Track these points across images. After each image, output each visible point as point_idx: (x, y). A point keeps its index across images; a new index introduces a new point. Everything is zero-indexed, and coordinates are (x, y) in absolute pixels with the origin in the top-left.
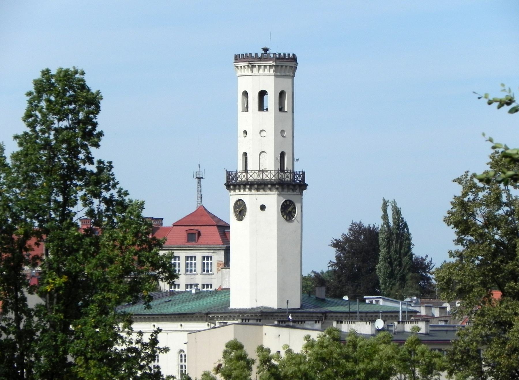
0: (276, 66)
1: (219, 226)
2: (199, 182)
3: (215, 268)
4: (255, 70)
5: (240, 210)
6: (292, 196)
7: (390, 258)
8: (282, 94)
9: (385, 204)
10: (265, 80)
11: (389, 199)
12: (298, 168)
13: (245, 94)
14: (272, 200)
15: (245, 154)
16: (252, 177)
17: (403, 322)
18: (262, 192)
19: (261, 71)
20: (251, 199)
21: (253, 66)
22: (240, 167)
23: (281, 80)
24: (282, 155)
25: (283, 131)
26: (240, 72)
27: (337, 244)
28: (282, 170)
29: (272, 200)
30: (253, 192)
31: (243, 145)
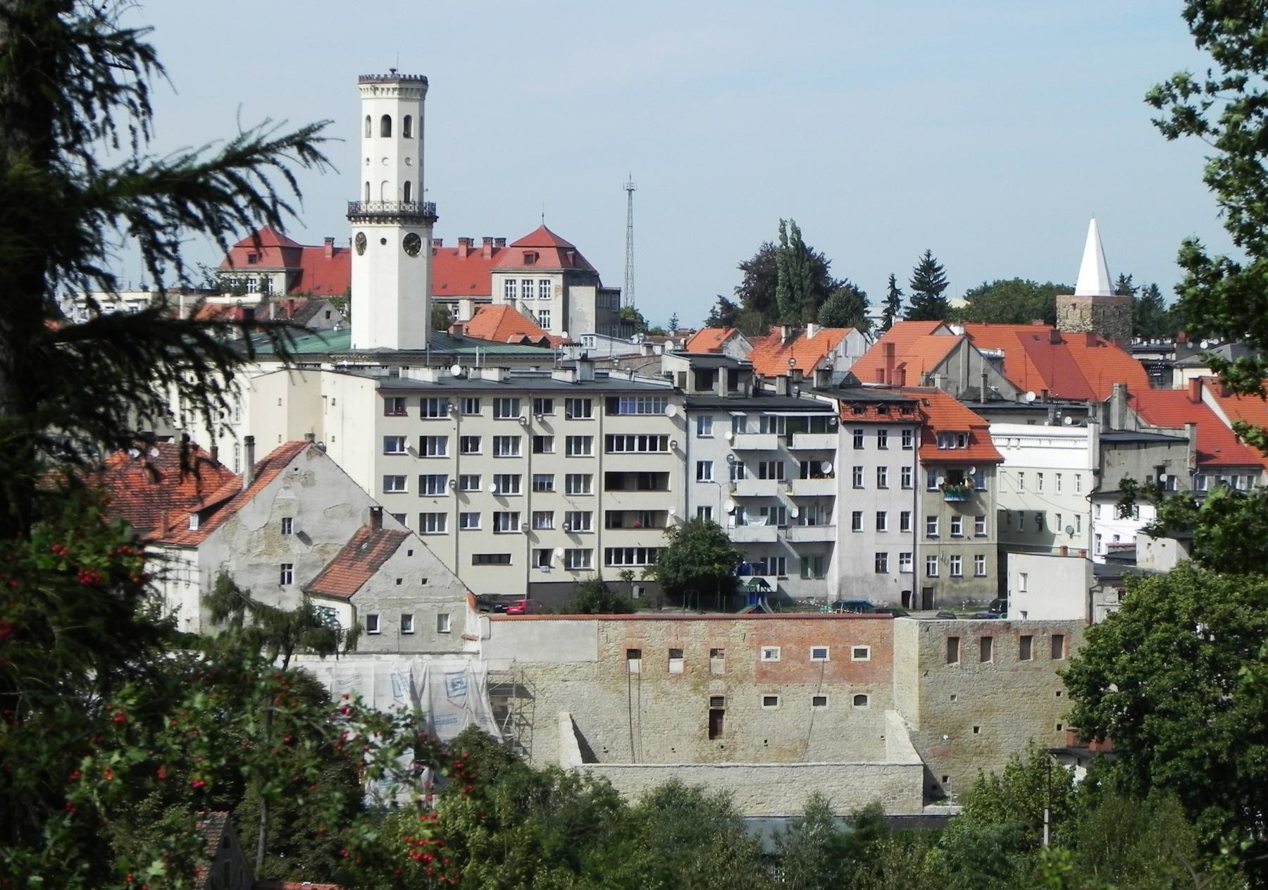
0: (400, 89)
1: (559, 248)
2: (630, 195)
3: (552, 293)
4: (378, 93)
5: (362, 243)
6: (419, 230)
7: (789, 281)
8: (407, 120)
9: (783, 224)
10: (389, 103)
11: (786, 218)
12: (427, 199)
13: (369, 118)
14: (394, 233)
15: (368, 183)
16: (374, 208)
17: (480, 369)
18: (383, 224)
19: (385, 94)
20: (372, 232)
21: (376, 89)
22: (363, 199)
23: (406, 104)
24: (407, 185)
25: (408, 159)
26: (364, 95)
27: (744, 267)
28: (407, 200)
29: (394, 233)
30: (374, 224)
31: (367, 174)
